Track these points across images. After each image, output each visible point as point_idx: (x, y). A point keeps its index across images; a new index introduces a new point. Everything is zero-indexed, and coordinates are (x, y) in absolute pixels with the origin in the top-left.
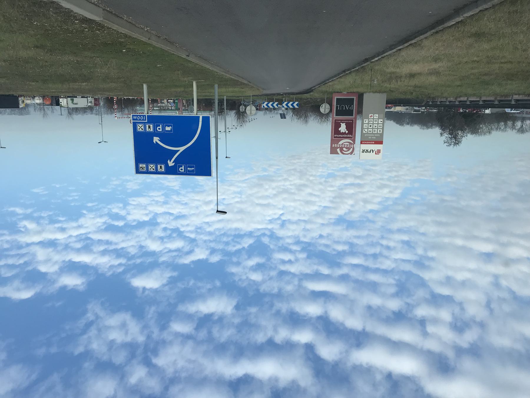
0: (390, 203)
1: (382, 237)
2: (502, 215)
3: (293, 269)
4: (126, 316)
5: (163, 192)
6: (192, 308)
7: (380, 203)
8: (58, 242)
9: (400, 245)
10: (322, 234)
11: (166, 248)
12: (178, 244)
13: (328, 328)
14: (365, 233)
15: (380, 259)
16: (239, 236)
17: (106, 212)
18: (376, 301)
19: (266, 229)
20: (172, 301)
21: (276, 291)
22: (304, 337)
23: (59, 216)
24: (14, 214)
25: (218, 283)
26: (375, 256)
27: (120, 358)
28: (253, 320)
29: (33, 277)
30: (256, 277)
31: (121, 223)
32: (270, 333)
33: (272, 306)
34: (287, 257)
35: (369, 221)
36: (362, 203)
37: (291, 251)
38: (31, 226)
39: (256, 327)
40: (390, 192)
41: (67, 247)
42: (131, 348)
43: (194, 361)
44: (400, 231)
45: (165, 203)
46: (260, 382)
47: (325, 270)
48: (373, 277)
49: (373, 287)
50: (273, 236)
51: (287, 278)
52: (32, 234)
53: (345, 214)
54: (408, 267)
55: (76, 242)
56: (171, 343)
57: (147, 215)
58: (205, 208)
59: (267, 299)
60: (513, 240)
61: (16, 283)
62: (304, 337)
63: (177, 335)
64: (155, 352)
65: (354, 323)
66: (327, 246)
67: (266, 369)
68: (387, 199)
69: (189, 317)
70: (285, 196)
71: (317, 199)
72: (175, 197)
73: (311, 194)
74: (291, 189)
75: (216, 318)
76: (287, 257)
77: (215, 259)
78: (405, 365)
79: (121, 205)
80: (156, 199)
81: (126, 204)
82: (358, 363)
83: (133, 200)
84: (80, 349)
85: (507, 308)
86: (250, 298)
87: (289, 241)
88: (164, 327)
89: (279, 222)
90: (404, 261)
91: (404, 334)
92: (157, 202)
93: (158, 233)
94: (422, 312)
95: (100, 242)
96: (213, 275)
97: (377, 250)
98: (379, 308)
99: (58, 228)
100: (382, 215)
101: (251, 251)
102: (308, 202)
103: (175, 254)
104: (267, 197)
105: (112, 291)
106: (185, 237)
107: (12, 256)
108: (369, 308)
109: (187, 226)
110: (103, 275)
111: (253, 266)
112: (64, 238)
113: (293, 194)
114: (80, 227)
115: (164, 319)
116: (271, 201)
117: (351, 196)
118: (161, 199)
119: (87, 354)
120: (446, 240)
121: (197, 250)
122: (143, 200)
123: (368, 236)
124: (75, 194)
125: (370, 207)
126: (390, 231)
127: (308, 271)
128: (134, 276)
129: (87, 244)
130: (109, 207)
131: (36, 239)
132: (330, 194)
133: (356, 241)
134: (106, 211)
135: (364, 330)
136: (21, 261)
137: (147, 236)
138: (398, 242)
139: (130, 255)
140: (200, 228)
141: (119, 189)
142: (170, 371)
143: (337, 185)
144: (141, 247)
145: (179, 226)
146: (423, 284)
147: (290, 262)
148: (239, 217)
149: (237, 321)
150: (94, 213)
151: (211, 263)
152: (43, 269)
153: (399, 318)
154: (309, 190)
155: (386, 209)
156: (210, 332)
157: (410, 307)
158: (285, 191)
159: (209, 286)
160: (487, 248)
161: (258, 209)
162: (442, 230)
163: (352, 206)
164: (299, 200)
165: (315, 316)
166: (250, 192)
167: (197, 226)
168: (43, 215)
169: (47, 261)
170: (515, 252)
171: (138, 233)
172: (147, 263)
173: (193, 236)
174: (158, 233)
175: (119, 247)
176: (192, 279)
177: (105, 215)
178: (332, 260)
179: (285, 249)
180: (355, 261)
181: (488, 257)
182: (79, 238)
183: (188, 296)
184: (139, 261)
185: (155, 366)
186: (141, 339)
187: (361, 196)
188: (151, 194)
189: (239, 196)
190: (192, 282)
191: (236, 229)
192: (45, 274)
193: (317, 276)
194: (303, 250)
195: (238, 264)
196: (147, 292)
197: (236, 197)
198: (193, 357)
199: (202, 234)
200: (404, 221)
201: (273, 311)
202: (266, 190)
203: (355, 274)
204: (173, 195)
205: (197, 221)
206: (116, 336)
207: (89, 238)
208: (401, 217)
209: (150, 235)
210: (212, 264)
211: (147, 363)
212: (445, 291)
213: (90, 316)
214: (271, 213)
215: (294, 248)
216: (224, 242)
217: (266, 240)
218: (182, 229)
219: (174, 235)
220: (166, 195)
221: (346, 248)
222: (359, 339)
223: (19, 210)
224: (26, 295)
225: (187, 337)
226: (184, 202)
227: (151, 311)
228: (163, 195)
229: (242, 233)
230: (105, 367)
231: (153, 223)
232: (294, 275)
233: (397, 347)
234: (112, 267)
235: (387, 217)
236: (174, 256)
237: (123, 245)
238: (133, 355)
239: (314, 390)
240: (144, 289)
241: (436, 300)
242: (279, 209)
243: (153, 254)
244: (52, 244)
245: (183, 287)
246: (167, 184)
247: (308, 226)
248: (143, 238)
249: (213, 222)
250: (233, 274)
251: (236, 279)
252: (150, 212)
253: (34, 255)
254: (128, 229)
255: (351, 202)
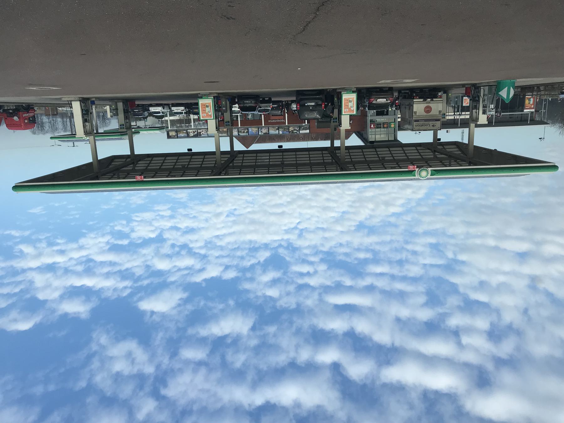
0: (414, 204)
1: (407, 242)
2: (534, 211)
3: (313, 282)
4: (131, 345)
5: (169, 206)
6: (203, 332)
7: (402, 205)
8: (57, 265)
9: (428, 250)
10: (341, 241)
11: (175, 266)
12: (188, 262)
13: (358, 344)
14: (388, 238)
15: (407, 267)
16: (254, 249)
17: (109, 231)
18: (405, 313)
19: (282, 240)
20: (180, 325)
21: (294, 306)
22: (328, 356)
23: (57, 238)
24: (11, 237)
25: (231, 302)
26: (400, 263)
27: (127, 390)
28: (272, 341)
29: (31, 304)
30: (273, 292)
31: (125, 242)
32: (292, 354)
33: (291, 323)
34: (305, 269)
35: (390, 224)
36: (383, 207)
37: (311, 263)
38: (27, 249)
39: (276, 348)
40: (414, 192)
41: (67, 271)
42: (140, 379)
43: (208, 391)
44: (426, 233)
45: (172, 217)
46: (285, 410)
47: (348, 282)
48: (399, 286)
49: (402, 296)
50: (291, 248)
51: (305, 293)
52: (31, 259)
53: (366, 219)
54: (435, 273)
55: (76, 265)
56: (181, 370)
57: (153, 231)
58: (215, 220)
59: (285, 317)
60: (549, 238)
61: (14, 314)
62: (328, 356)
63: (187, 362)
64: (164, 384)
65: (383, 337)
66: (346, 254)
67: (289, 393)
68: (409, 200)
69: (203, 341)
70: (300, 203)
71: (335, 205)
72: (181, 210)
73: (328, 200)
74: (307, 195)
75: (229, 341)
76: (305, 269)
77: (231, 275)
78: (441, 381)
79: (124, 222)
80: (161, 213)
81: (129, 220)
82: (387, 381)
83: (137, 216)
84: (83, 384)
85: (545, 313)
86: (267, 314)
87: (306, 251)
88: (174, 354)
89: (297, 232)
90: (432, 266)
91: (437, 347)
92: (162, 217)
93: (166, 249)
94: (454, 321)
95: (102, 263)
96: (224, 293)
97: (404, 256)
98: (409, 319)
99: (57, 251)
100: (405, 218)
101: (266, 265)
102: (325, 209)
103: (186, 272)
104: (281, 205)
105: (121, 316)
106: (195, 254)
107: (8, 284)
108: (398, 320)
109: (197, 242)
110: (106, 299)
111: (267, 282)
112: (64, 262)
113: (310, 200)
114: (81, 248)
115: (174, 346)
116: (285, 209)
117: (370, 199)
118: (168, 213)
119: (90, 388)
120: (478, 241)
121: (209, 267)
122: (147, 216)
123: (391, 242)
124: (75, 212)
125: (393, 210)
126: (416, 235)
127: (328, 283)
128: (141, 299)
129: (89, 267)
130: (111, 224)
131: (34, 264)
132: (349, 198)
133: (378, 248)
134: (108, 229)
135: (393, 344)
136: (17, 290)
137: (153, 254)
138: (424, 246)
139: (136, 277)
140: (210, 242)
141: (124, 204)
142: (182, 402)
143: (356, 188)
144: (148, 267)
145: (188, 242)
146: (454, 289)
147: (308, 274)
148: (252, 228)
149: (254, 342)
150: (96, 232)
151: (225, 280)
152: (41, 296)
153: (432, 328)
154: (325, 196)
155: (408, 211)
156: (223, 357)
157: (443, 317)
158: (300, 197)
159: (221, 306)
160: (524, 247)
161: (273, 219)
162: (473, 230)
163: (373, 210)
164: (316, 206)
165: (341, 332)
166: (263, 201)
167: (206, 240)
168: (41, 237)
169: (48, 286)
170: (550, 249)
171: (144, 251)
172: (157, 283)
173: (203, 252)
174: (166, 249)
175: (123, 268)
176: (209, 297)
177: (108, 233)
178: (355, 269)
179: (304, 261)
180: (379, 269)
181: (523, 256)
182: (79, 262)
183: (199, 317)
184: (146, 282)
185: (164, 398)
186: (150, 370)
187: (384, 198)
188: (156, 209)
189: (252, 205)
190: (202, 303)
191: (251, 242)
192: (45, 302)
193: (338, 288)
194: (322, 260)
195: (252, 280)
196: (154, 317)
197: (248, 207)
198: (207, 386)
199: (212, 249)
200: (430, 223)
201: (294, 329)
202: (281, 197)
203: (381, 283)
204: (179, 208)
205: (207, 235)
206: (119, 366)
207: (91, 260)
208: (427, 219)
209: (157, 253)
210: (225, 281)
211: (156, 395)
212: (482, 297)
213: (94, 347)
214: (289, 222)
215: (312, 259)
216: (239, 257)
217: (281, 251)
218: (191, 245)
219: (183, 252)
220: (172, 209)
221: (369, 255)
222: (387, 355)
223: (14, 233)
224: (24, 326)
225: (200, 364)
226: (192, 216)
227: (159, 337)
228: (169, 209)
229: (257, 245)
230: (109, 402)
231: (160, 240)
232: (313, 288)
233: (430, 361)
234: (115, 290)
235: (409, 219)
236: (185, 275)
237: (128, 265)
238: (141, 387)
239: (342, 415)
240: (153, 313)
241: (470, 306)
242: (296, 217)
243: (160, 273)
244: (51, 268)
245: (193, 308)
246: (174, 196)
247: (327, 235)
248: (150, 258)
249: (224, 235)
250: (247, 291)
251: (252, 296)
252: (157, 228)
253: (31, 282)
254: (133, 247)
255: (371, 206)
